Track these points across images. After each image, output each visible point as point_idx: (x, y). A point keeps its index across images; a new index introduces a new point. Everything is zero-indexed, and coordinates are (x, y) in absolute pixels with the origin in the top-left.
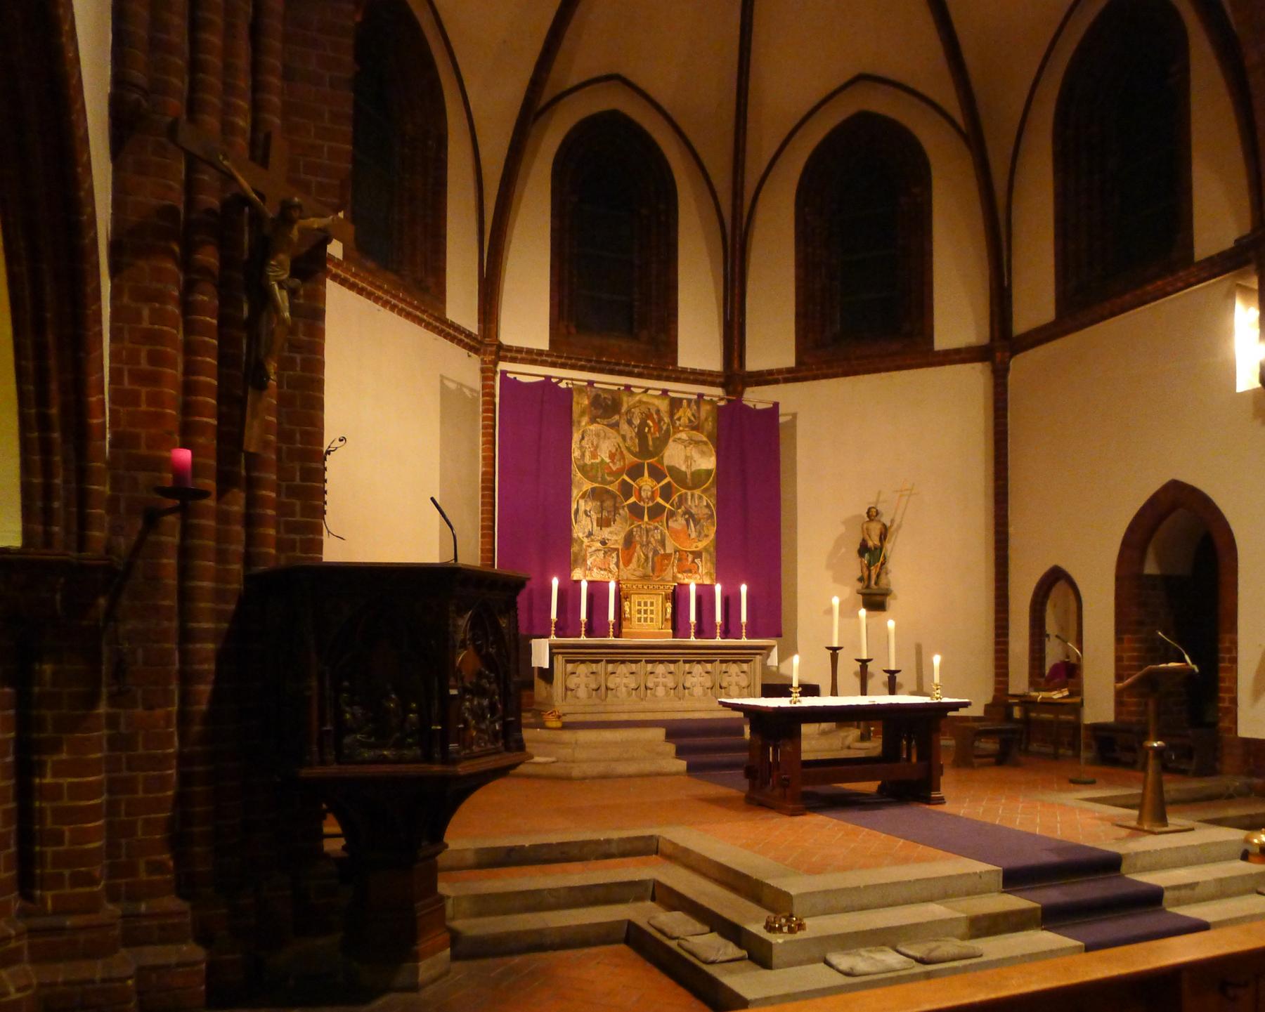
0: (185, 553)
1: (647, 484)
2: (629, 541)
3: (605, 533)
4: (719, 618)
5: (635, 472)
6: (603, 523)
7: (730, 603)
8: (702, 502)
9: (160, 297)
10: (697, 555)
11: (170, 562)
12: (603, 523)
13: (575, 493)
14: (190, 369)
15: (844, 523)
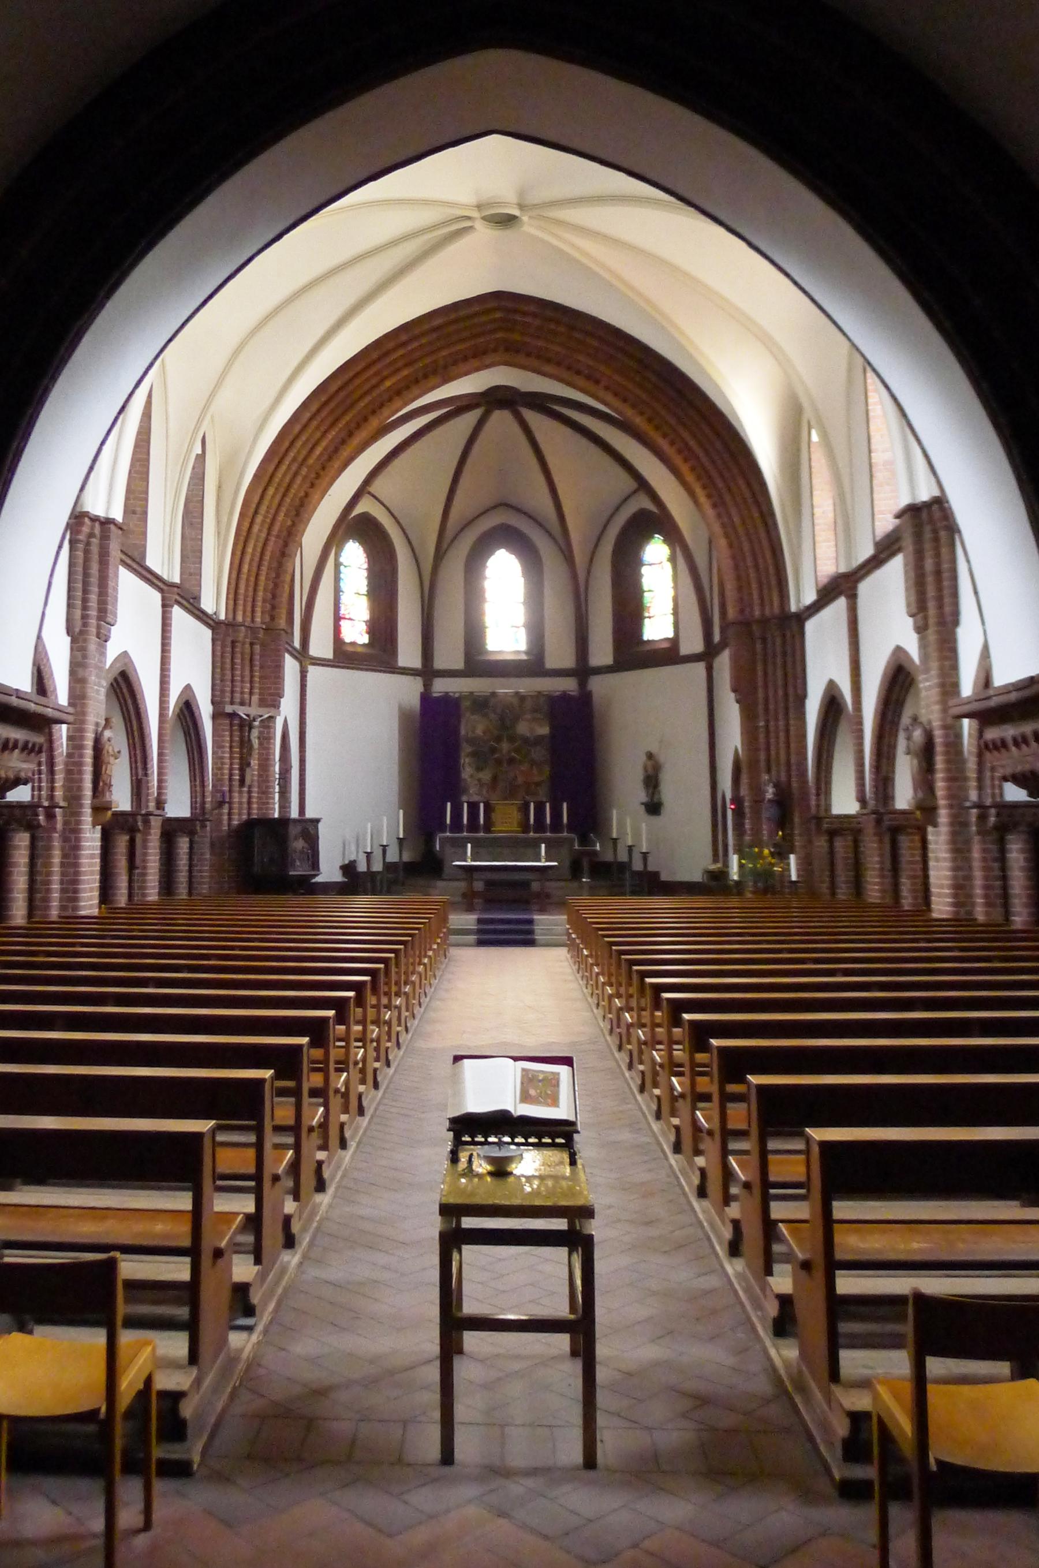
0: (230, 814)
1: (505, 746)
2: (495, 779)
3: (481, 775)
4: (482, 821)
5: (499, 739)
6: (479, 769)
7: (556, 814)
8: (539, 753)
9: (223, 747)
10: (538, 784)
11: (226, 817)
12: (479, 769)
13: (463, 754)
14: (231, 764)
15: (317, 821)
